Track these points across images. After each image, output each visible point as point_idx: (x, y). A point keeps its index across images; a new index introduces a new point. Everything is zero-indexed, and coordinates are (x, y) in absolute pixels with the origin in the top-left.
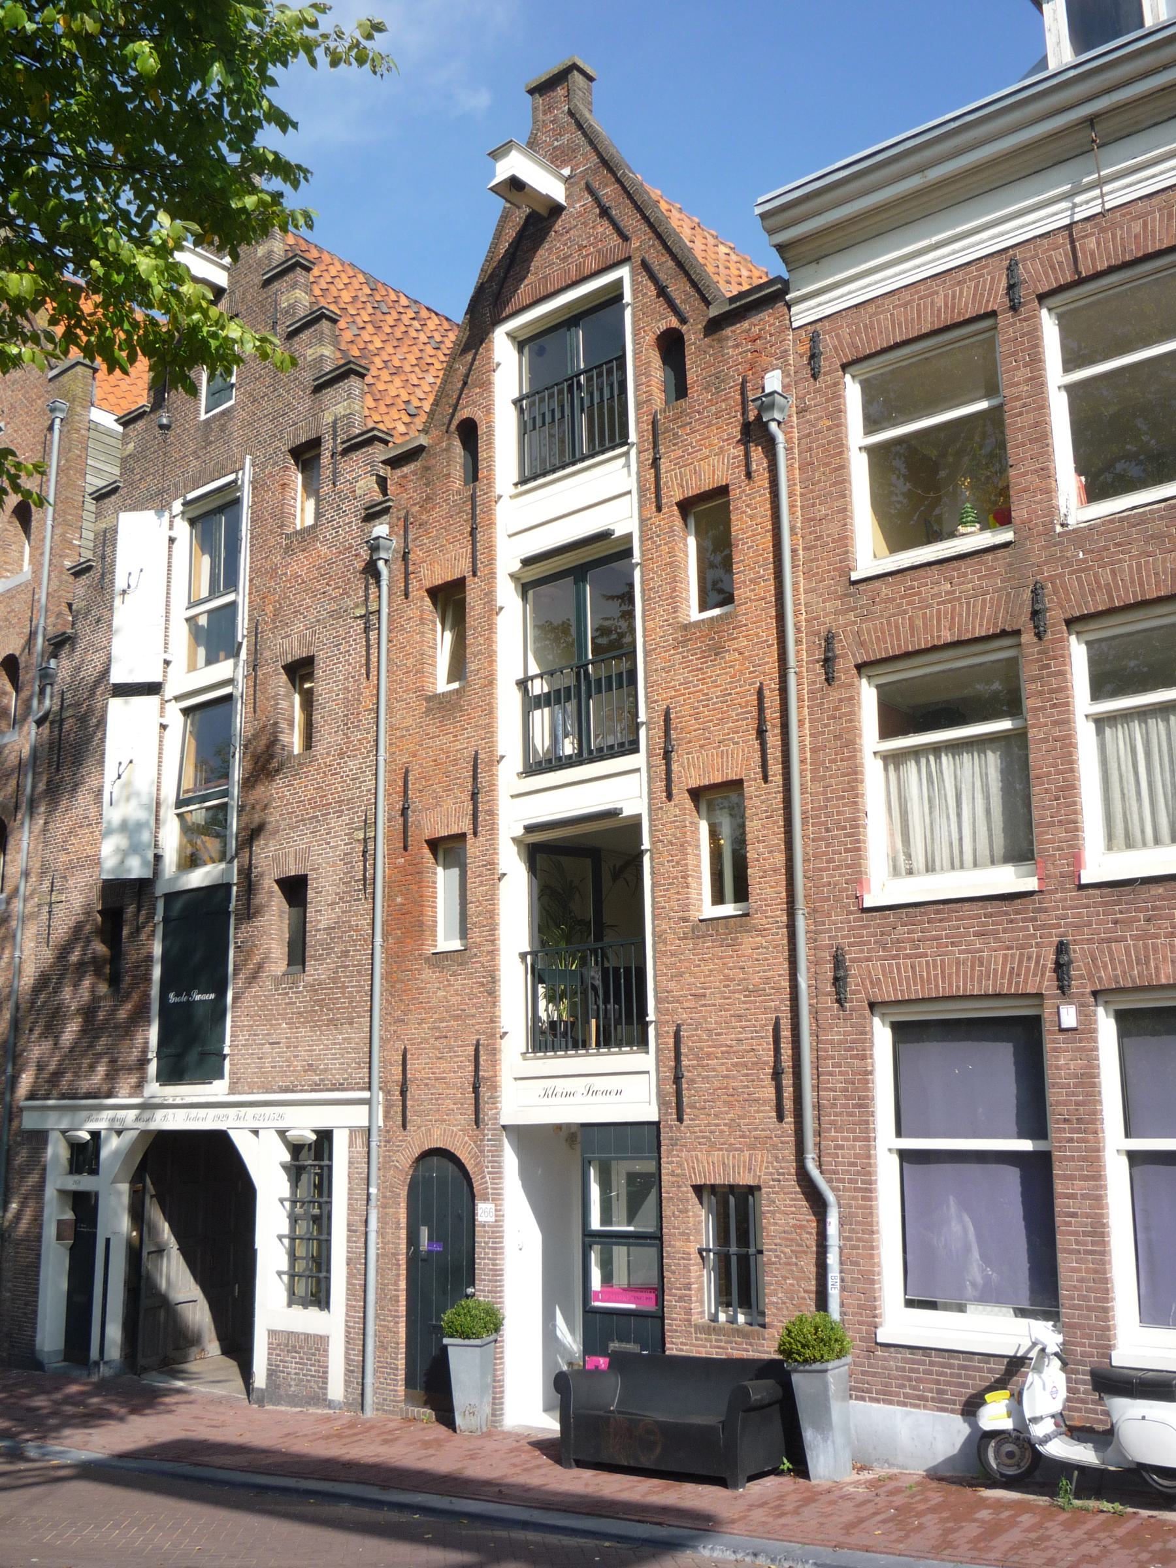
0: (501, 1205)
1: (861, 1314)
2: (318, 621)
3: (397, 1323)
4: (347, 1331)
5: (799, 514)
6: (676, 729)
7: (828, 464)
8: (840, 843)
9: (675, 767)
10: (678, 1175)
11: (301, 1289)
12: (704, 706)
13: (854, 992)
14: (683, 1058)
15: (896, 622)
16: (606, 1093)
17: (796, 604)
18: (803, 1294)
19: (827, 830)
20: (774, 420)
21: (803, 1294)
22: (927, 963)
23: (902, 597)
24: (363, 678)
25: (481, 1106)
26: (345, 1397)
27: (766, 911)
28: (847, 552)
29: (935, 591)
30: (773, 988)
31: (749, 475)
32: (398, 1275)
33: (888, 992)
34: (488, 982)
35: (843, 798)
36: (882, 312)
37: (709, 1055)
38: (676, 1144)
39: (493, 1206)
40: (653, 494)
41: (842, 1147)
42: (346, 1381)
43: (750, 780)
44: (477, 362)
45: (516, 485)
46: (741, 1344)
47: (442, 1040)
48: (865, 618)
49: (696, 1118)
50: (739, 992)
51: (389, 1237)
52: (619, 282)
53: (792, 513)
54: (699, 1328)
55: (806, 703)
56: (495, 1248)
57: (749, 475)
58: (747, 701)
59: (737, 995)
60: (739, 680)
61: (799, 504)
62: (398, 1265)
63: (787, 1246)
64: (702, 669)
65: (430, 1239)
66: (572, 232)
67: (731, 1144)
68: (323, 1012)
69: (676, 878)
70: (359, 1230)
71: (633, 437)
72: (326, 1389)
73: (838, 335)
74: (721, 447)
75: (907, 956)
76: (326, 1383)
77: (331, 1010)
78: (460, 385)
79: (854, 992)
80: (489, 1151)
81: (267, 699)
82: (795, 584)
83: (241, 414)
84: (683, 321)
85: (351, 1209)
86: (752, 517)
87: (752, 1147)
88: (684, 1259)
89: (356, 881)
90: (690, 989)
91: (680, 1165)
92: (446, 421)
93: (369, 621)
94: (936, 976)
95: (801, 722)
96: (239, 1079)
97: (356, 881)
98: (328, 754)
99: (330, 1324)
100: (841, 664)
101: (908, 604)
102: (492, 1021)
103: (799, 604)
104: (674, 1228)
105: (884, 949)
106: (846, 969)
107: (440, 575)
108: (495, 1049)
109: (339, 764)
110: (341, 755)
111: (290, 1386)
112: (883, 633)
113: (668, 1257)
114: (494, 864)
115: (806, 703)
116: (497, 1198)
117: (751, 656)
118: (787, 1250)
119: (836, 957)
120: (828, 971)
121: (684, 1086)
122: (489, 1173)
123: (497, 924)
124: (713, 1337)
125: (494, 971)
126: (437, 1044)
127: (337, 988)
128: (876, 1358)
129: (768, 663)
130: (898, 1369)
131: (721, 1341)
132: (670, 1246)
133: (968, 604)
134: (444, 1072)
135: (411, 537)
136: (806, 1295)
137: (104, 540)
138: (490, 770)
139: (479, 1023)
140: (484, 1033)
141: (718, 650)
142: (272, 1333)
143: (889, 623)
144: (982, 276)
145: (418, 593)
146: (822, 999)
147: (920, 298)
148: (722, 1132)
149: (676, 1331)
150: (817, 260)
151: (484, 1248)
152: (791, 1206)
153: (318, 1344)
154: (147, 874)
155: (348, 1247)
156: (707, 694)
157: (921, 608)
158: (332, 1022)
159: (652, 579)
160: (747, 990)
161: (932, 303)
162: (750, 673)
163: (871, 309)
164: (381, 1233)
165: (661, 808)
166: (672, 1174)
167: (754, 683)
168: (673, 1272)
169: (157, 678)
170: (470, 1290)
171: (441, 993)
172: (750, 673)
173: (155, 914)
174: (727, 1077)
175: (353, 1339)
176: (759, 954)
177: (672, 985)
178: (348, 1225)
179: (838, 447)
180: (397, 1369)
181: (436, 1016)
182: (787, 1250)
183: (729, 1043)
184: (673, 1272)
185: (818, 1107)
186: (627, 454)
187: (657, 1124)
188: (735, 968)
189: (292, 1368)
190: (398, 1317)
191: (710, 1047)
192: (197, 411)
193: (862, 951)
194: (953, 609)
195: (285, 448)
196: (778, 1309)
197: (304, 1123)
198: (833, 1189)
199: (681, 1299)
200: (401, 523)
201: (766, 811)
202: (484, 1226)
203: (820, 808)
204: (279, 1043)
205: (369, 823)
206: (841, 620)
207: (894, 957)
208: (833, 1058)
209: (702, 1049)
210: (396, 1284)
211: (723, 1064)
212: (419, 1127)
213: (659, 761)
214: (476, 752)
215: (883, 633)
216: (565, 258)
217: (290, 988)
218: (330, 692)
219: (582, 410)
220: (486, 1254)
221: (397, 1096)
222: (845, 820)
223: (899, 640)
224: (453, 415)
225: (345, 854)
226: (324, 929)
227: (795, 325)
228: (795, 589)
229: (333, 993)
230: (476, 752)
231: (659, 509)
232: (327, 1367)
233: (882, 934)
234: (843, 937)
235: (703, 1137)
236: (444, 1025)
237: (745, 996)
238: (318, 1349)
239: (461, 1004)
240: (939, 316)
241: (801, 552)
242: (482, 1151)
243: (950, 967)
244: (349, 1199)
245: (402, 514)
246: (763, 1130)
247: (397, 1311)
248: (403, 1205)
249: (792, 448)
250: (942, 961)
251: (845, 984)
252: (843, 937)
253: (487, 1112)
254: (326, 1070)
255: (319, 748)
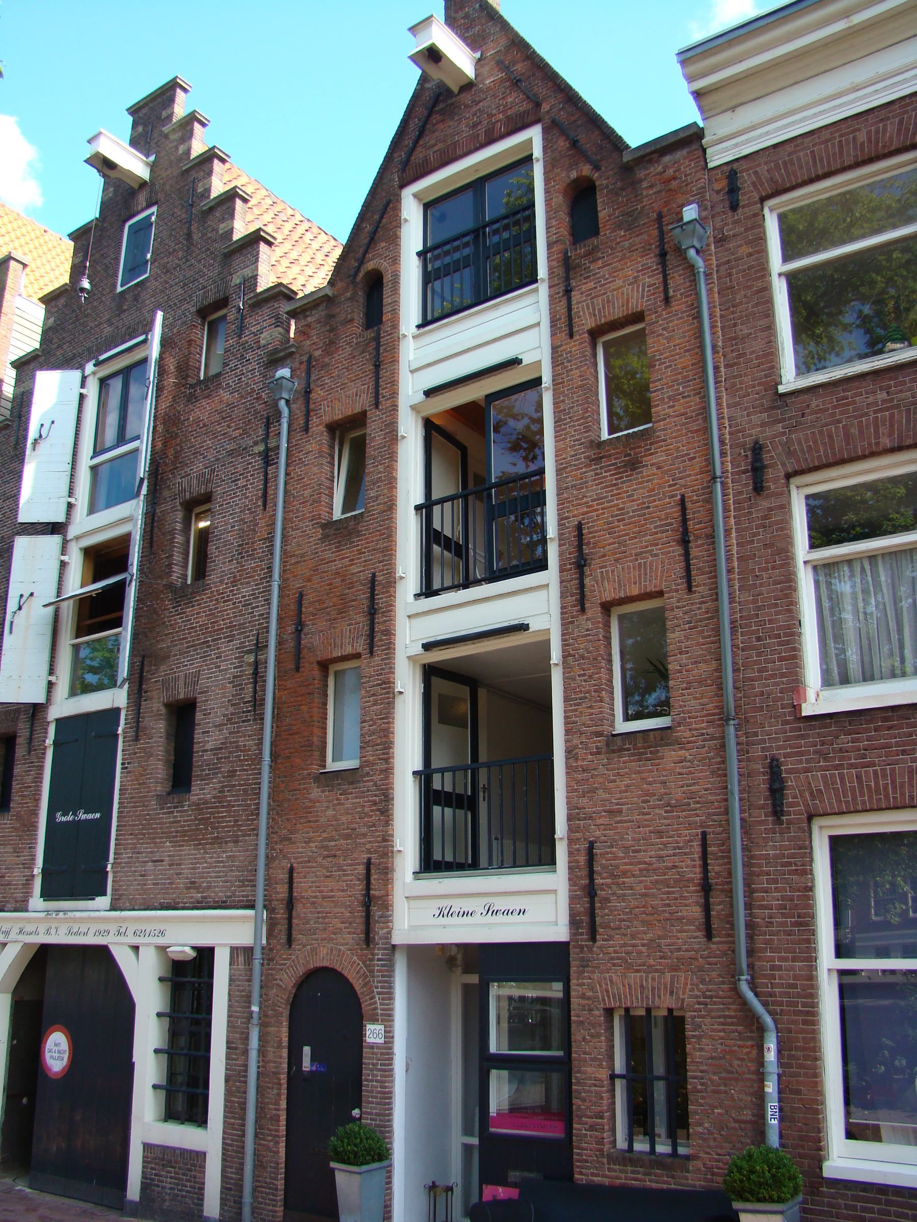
0: (391, 1026)
1: (803, 1147)
2: (217, 460)
3: (278, 1142)
4: (223, 1149)
5: (720, 333)
6: (589, 543)
7: (750, 287)
8: (773, 652)
9: (587, 581)
10: (589, 998)
11: (180, 1104)
12: (619, 521)
13: (792, 805)
14: (595, 876)
15: (830, 431)
16: (507, 912)
17: (720, 418)
18: (733, 1125)
19: (759, 639)
20: (693, 247)
21: (733, 1125)
22: (875, 772)
23: (836, 407)
24: (259, 510)
25: (372, 925)
26: (221, 1215)
27: (690, 724)
28: (773, 367)
29: (871, 399)
30: (698, 802)
31: (667, 300)
32: (279, 1094)
33: (831, 804)
34: (381, 801)
35: (776, 605)
36: (803, 149)
37: (625, 874)
38: (587, 966)
39: (382, 1027)
40: (564, 323)
41: (780, 968)
42: (222, 1199)
43: (671, 591)
44: (384, 220)
45: (419, 327)
46: (662, 1176)
47: (330, 859)
48: (793, 429)
49: (611, 938)
50: (658, 807)
51: (271, 1056)
52: (530, 141)
53: (713, 334)
54: (611, 1159)
55: (732, 513)
56: (385, 1070)
57: (667, 300)
58: (667, 514)
59: (657, 811)
60: (659, 494)
61: (719, 324)
62: (280, 1084)
63: (714, 1073)
64: (616, 485)
65: (313, 1059)
66: (481, 104)
67: (650, 966)
68: (205, 831)
69: (588, 692)
70: (236, 1048)
71: (542, 271)
72: (202, 1205)
73: (756, 173)
74: (635, 278)
75: (852, 766)
76: (202, 1200)
77: (217, 828)
78: (366, 241)
79: (792, 805)
80: (378, 971)
81: (164, 534)
82: (718, 398)
83: (154, 284)
84: (597, 168)
85: (231, 1026)
86: (669, 339)
87: (674, 968)
88: (595, 1085)
89: (245, 703)
90: (604, 805)
91: (592, 989)
92: (352, 272)
93: (268, 458)
94: (886, 786)
95: (727, 532)
96: (122, 895)
97: (245, 703)
98: (221, 582)
99: (208, 1139)
100: (770, 474)
101: (842, 413)
102: (385, 840)
103: (723, 418)
104: (585, 1053)
105: (825, 759)
106: (782, 781)
107: (339, 410)
108: (387, 868)
109: (232, 591)
110: (234, 582)
111: (164, 1201)
112: (815, 442)
113: (578, 1083)
114: (389, 682)
115: (732, 513)
116: (387, 1019)
117: (670, 470)
118: (715, 1078)
119: (771, 766)
120: (761, 782)
121: (597, 905)
122: (379, 993)
123: (392, 743)
124: (629, 1168)
125: (387, 789)
126: (325, 862)
127: (223, 807)
128: (820, 1194)
129: (690, 475)
130: (847, 1207)
131: (638, 1173)
132: (579, 1072)
133: (908, 411)
134: (332, 891)
135: (313, 377)
136: (737, 1125)
137: (22, 402)
138: (388, 592)
139: (370, 842)
140: (376, 852)
141: (633, 465)
142: (147, 1147)
143: (821, 432)
144: (906, 112)
145: (318, 428)
146: (756, 812)
147: (841, 136)
148: (640, 953)
149: (587, 1161)
150: (733, 109)
151: (372, 1070)
152: (720, 1031)
153: (198, 1158)
154: (40, 698)
155: (227, 1064)
156: (623, 509)
157: (856, 417)
158: (218, 841)
159: (563, 401)
160: (669, 805)
161: (854, 139)
162: (670, 486)
163: (789, 148)
164: (262, 1052)
165: (572, 622)
166: (583, 996)
167: (676, 495)
168: (584, 1100)
169: (61, 518)
170: (356, 1112)
171: (330, 812)
172: (670, 486)
173: (46, 737)
174: (645, 895)
175: (230, 1156)
176: (683, 767)
177: (584, 801)
178: (228, 1042)
179: (763, 270)
180: (276, 1189)
181: (324, 835)
182: (715, 1078)
183: (647, 860)
184: (584, 1100)
185: (750, 925)
186: (536, 290)
187: (565, 945)
188: (655, 782)
189: (168, 1183)
190: (278, 1136)
191: (626, 864)
192: (114, 286)
193: (801, 761)
194: (892, 416)
195: (194, 309)
196: (704, 1140)
197: (185, 931)
198: (770, 1013)
199: (592, 1128)
200: (304, 367)
201: (690, 622)
202: (372, 1047)
203: (749, 617)
204: (162, 861)
205: (260, 647)
206: (769, 432)
207: (836, 767)
208: (768, 874)
209: (617, 867)
210: (277, 1103)
211: (641, 882)
212: (304, 946)
213: (573, 574)
214: (374, 575)
215: (815, 442)
216: (475, 126)
217: (175, 807)
218: (226, 524)
219: (484, 800)
220: (373, 1075)
221: (281, 914)
222: (779, 628)
223: (832, 448)
224: (358, 269)
225: (234, 677)
226: (211, 750)
227: (711, 165)
228: (719, 404)
229: (218, 812)
230: (374, 575)
231: (571, 336)
232: (204, 1183)
233: (823, 743)
234: (779, 748)
235: (618, 958)
236: (333, 843)
237: (666, 812)
238: (195, 1165)
239: (352, 823)
240: (862, 150)
241: (722, 369)
242: (372, 971)
243: (902, 776)
244: (229, 1016)
245: (305, 358)
246: (687, 950)
247: (277, 1131)
248: (285, 1024)
249: (711, 274)
250: (893, 770)
251: (782, 796)
252: (779, 748)
253: (379, 931)
254: (209, 887)
255: (213, 578)
